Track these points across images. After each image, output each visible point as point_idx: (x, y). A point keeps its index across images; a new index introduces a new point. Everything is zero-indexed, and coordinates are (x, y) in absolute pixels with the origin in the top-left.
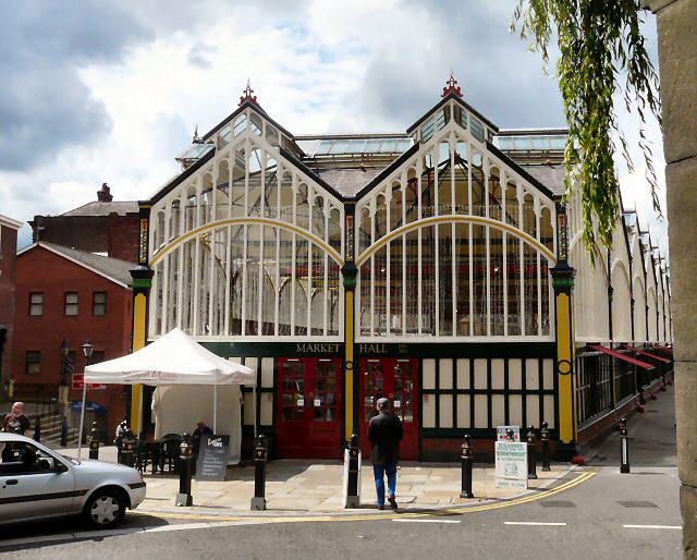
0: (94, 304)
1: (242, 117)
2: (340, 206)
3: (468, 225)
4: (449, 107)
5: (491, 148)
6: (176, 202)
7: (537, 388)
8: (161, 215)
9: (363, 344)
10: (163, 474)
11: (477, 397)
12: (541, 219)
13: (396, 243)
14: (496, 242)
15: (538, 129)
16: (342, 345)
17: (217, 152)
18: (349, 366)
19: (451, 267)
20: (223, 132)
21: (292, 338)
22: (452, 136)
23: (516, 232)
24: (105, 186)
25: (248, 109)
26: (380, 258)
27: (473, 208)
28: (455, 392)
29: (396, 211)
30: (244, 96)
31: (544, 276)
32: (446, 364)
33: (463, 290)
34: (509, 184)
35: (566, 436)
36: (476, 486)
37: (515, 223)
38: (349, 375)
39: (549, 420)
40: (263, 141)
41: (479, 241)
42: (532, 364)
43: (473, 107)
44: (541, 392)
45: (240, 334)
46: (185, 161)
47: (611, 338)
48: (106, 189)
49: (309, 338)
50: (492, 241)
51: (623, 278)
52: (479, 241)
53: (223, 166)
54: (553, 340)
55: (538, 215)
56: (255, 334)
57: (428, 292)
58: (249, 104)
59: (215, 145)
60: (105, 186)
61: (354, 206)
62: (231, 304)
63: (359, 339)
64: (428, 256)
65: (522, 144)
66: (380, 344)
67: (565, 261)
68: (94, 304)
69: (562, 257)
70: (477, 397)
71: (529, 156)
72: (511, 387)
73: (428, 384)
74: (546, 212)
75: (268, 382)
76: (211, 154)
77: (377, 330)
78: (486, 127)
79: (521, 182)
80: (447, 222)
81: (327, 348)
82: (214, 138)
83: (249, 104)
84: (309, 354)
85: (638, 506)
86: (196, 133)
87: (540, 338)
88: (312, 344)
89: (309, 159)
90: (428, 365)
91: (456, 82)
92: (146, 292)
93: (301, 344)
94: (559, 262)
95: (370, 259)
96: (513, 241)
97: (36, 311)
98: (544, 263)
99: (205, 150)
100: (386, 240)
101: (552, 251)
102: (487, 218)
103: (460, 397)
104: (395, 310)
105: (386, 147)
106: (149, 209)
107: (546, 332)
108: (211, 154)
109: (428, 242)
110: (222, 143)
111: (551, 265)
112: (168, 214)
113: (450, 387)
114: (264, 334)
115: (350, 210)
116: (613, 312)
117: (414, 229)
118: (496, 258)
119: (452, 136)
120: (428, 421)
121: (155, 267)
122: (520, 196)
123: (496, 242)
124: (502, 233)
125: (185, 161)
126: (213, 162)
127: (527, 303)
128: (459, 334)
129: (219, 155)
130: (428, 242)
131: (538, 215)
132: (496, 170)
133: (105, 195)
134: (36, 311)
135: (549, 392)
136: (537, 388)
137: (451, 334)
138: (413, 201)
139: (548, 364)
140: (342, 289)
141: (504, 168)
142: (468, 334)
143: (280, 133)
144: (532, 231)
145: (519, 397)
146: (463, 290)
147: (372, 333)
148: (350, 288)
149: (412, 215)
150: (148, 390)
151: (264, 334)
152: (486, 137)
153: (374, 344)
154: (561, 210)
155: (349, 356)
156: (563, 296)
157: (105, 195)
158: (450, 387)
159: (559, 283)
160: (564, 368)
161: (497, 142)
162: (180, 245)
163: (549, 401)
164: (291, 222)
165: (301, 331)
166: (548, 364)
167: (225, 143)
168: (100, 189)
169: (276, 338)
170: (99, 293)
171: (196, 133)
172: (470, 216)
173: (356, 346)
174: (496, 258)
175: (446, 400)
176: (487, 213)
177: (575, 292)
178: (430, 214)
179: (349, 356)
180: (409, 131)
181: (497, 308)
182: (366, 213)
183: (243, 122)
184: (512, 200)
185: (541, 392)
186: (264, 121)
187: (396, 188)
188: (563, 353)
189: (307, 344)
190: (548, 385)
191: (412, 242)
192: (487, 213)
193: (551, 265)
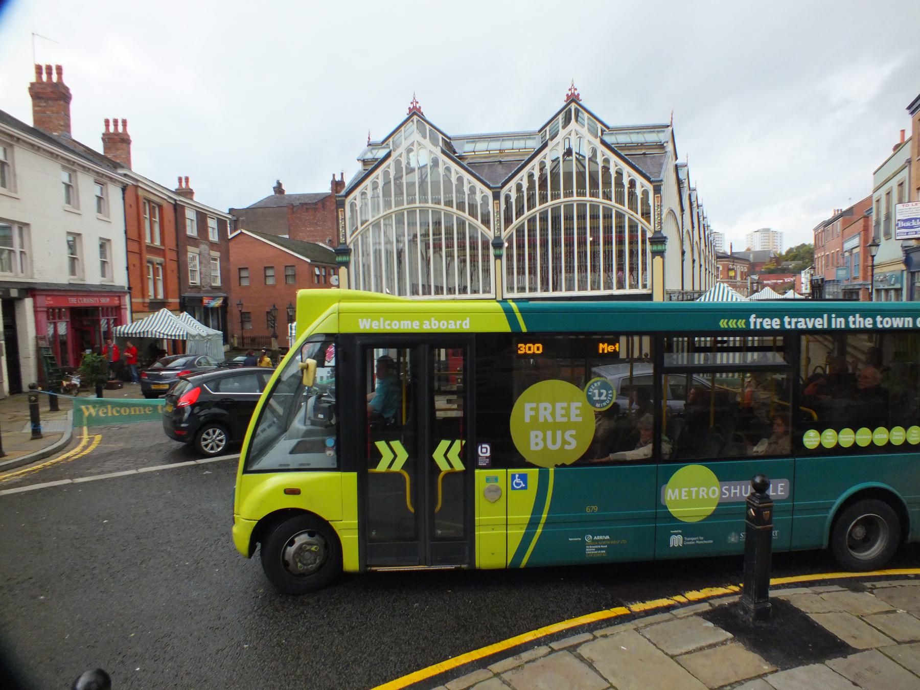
0: (240, 278)
1: (410, 124)
2: (650, 187)
3: (599, 206)
5: (603, 143)
6: (363, 194)
8: (353, 205)
12: (642, 199)
13: (532, 220)
14: (607, 217)
17: (393, 153)
20: (396, 136)
22: (573, 133)
25: (415, 118)
26: (520, 231)
27: (590, 192)
29: (531, 198)
31: (644, 242)
33: (556, 258)
34: (617, 172)
37: (622, 203)
40: (427, 142)
46: (365, 162)
48: (279, 184)
50: (604, 217)
51: (689, 243)
52: (594, 217)
53: (398, 163)
54: (650, 292)
55: (640, 196)
56: (599, 288)
57: (532, 258)
58: (415, 112)
59: (391, 148)
61: (499, 193)
64: (544, 230)
65: (623, 139)
67: (660, 232)
68: (266, 276)
69: (497, 234)
71: (626, 147)
74: (485, 198)
76: (388, 156)
78: (599, 126)
80: (570, 203)
83: (415, 112)
85: (65, 446)
86: (369, 138)
87: (640, 291)
91: (576, 89)
92: (661, 253)
94: (655, 232)
95: (512, 234)
96: (620, 216)
97: (270, 281)
102: (613, 203)
106: (344, 200)
107: (645, 286)
108: (388, 156)
109: (556, 219)
110: (396, 146)
111: (649, 235)
112: (358, 203)
114: (604, 289)
115: (496, 196)
117: (546, 209)
118: (608, 229)
119: (573, 133)
121: (352, 247)
122: (626, 181)
123: (607, 217)
124: (611, 210)
125: (365, 162)
126: (390, 161)
129: (394, 155)
130: (556, 219)
131: (640, 196)
133: (279, 189)
134: (270, 281)
137: (586, 289)
138: (543, 185)
141: (613, 159)
143: (440, 136)
146: (556, 258)
148: (498, 257)
149: (544, 199)
150: (184, 342)
151: (604, 289)
152: (600, 134)
154: (657, 190)
156: (658, 259)
157: (279, 189)
159: (655, 248)
161: (609, 139)
162: (515, 222)
167: (398, 147)
168: (275, 184)
170: (243, 269)
171: (369, 138)
176: (430, 201)
177: (666, 254)
178: (571, 194)
181: (582, 268)
182: (508, 198)
183: (412, 126)
184: (619, 184)
186: (428, 126)
187: (531, 176)
191: (544, 219)
192: (430, 201)
193: (649, 235)
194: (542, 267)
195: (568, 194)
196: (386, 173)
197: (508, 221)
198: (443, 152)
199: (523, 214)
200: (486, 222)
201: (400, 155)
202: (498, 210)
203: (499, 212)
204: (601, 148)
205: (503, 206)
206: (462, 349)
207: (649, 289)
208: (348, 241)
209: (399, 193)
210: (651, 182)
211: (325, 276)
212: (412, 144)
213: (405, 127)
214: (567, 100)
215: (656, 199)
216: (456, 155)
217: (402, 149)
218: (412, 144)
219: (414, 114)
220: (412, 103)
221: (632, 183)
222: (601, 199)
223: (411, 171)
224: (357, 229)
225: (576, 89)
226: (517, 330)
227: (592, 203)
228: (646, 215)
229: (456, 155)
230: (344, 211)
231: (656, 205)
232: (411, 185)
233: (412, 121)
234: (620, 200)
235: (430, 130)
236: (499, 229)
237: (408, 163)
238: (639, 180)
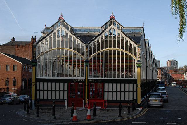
1: (59, 22)
2: (85, 45)
3: (116, 51)
4: (111, 21)
5: (122, 32)
7: (43, 89)
9: (90, 79)
11: (113, 93)
13: (98, 54)
14: (119, 54)
16: (85, 80)
18: (86, 85)
19: (130, 60)
21: (72, 78)
24: (13, 37)
25: (61, 21)
26: (94, 58)
28: (112, 91)
30: (111, 16)
31: (134, 63)
32: (110, 85)
35: (139, 102)
36: (57, 116)
38: (86, 87)
39: (135, 98)
41: (114, 54)
42: (131, 85)
43: (118, 21)
44: (133, 92)
45: (59, 77)
48: (14, 38)
49: (76, 78)
58: (61, 19)
60: (13, 37)
62: (53, 69)
63: (89, 78)
66: (94, 80)
69: (34, 58)
70: (113, 93)
72: (48, 89)
73: (106, 89)
74: (83, 47)
75: (66, 89)
77: (49, 76)
81: (81, 80)
84: (76, 82)
87: (133, 79)
88: (77, 79)
90: (106, 85)
93: (74, 79)
95: (92, 59)
98: (134, 60)
101: (134, 59)
102: (117, 48)
103: (61, 92)
110: (55, 29)
111: (136, 61)
113: (107, 90)
114: (122, 77)
118: (123, 59)
120: (106, 99)
121: (37, 60)
123: (119, 54)
132: (123, 37)
135: (135, 92)
136: (59, 89)
139: (135, 85)
140: (85, 66)
142: (59, 77)
145: (54, 92)
147: (92, 76)
148: (87, 66)
151: (122, 77)
153: (93, 80)
155: (87, 82)
158: (46, 89)
159: (138, 65)
160: (139, 86)
163: (135, 93)
164: (76, 51)
165: (74, 76)
166: (135, 85)
168: (12, 38)
169: (68, 78)
172: (65, 48)
173: (88, 80)
174: (123, 59)
175: (110, 93)
179: (87, 82)
185: (133, 92)
186: (65, 23)
188: (139, 82)
189: (76, 79)
190: (135, 90)
193: (136, 61)
196: (50, 37)
197: (90, 54)
200: (135, 54)
203: (87, 52)
204: (69, 33)
205: (89, 50)
208: (37, 58)
209: (54, 44)
211: (27, 69)
217: (56, 30)
218: (60, 29)
223: (59, 37)
224: (40, 54)
228: (135, 54)
230: (36, 48)
232: (59, 42)
233: (60, 22)
236: (87, 57)
237: (58, 34)
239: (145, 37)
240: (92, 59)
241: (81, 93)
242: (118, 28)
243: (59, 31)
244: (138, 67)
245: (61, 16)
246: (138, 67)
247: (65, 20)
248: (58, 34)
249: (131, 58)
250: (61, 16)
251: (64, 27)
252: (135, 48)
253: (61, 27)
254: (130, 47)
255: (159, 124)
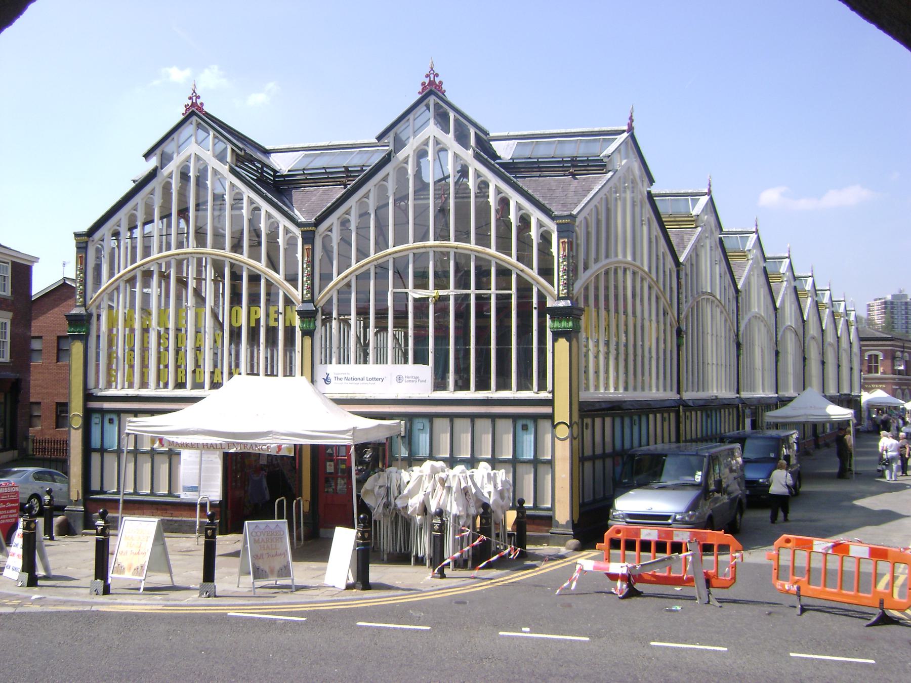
1: (422, 107)
2: (552, 226)
6: (345, 223)
8: (326, 239)
10: (627, 571)
14: (236, 277)
15: (568, 131)
23: (509, 263)
47: (738, 392)
54: (550, 396)
74: (545, 238)
79: (515, 199)
82: (389, 139)
89: (282, 176)
92: (85, 339)
99: (154, 162)
100: (351, 273)
102: (492, 251)
104: (421, 358)
105: (354, 160)
110: (399, 144)
115: (309, 238)
116: (779, 370)
123: (236, 277)
126: (155, 184)
127: (457, 351)
128: (520, 388)
142: (468, 389)
144: (273, 264)
163: (96, 442)
164: (510, 255)
180: (379, 138)
194: (498, 352)
195: (443, 235)
198: (477, 157)
199: (350, 266)
200: (546, 272)
201: (406, 161)
202: (310, 259)
204: (475, 166)
206: (499, 489)
207: (549, 392)
210: (553, 218)
212: (426, 143)
213: (415, 115)
214: (423, 91)
215: (561, 244)
216: (498, 161)
217: (408, 151)
218: (426, 143)
219: (431, 93)
220: (427, 76)
221: (525, 221)
222: (472, 245)
225: (437, 75)
226: (908, 468)
227: (459, 251)
228: (546, 272)
229: (498, 161)
231: (561, 256)
234: (504, 246)
235: (456, 120)
236: (311, 289)
237: (418, 175)
238: (536, 216)
239: (651, 181)
240: (335, 301)
241: (625, 483)
242: (462, 138)
243: (421, 154)
244: (557, 335)
245: (432, 73)
246: (557, 335)
247: (449, 97)
248: (418, 175)
249: (525, 289)
250: (432, 73)
251: (447, 132)
252: (545, 238)
253: (432, 130)
254: (520, 230)
255: (652, 646)
